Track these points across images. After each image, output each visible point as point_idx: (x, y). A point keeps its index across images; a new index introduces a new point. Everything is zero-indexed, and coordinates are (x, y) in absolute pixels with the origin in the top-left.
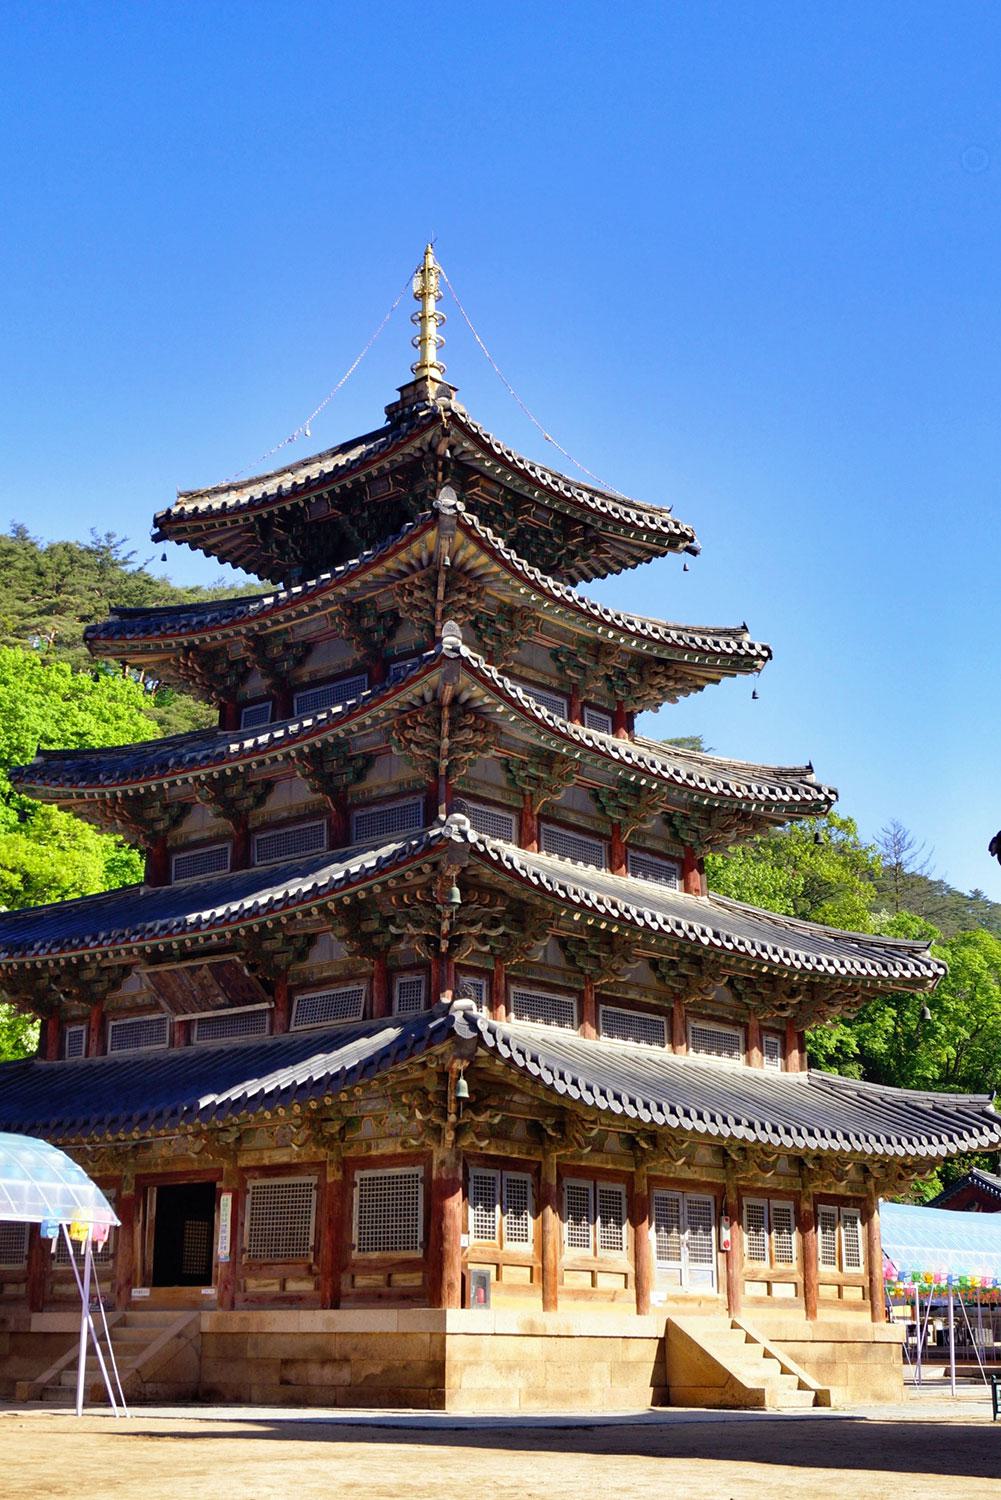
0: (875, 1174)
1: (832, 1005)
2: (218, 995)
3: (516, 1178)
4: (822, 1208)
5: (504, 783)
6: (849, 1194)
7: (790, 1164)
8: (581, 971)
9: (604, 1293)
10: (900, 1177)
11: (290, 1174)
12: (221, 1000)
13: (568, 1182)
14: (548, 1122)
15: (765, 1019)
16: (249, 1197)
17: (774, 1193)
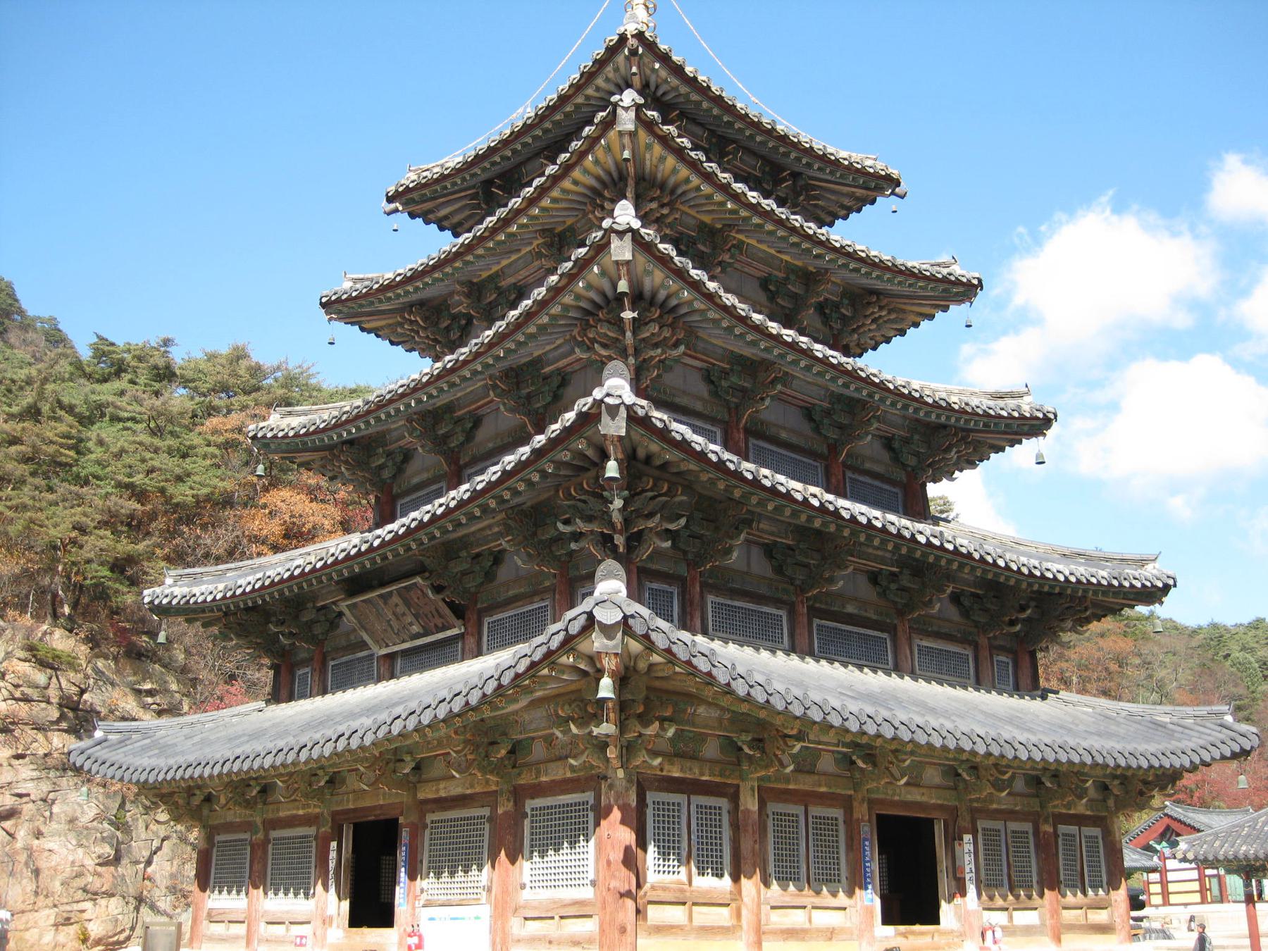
0: (1116, 792)
1: (1062, 620)
2: (411, 624)
3: (709, 804)
4: (1063, 829)
5: (706, 395)
6: (1088, 813)
7: (1027, 783)
8: (791, 581)
9: (819, 930)
10: (1141, 793)
11: (464, 806)
12: (415, 629)
13: (772, 807)
14: (743, 738)
15: (995, 637)
16: (427, 832)
17: (1010, 815)
